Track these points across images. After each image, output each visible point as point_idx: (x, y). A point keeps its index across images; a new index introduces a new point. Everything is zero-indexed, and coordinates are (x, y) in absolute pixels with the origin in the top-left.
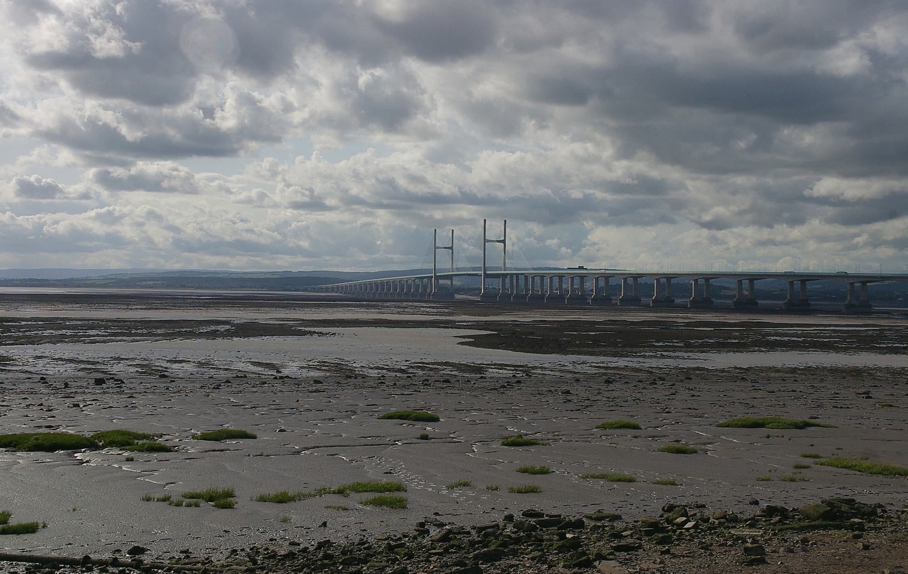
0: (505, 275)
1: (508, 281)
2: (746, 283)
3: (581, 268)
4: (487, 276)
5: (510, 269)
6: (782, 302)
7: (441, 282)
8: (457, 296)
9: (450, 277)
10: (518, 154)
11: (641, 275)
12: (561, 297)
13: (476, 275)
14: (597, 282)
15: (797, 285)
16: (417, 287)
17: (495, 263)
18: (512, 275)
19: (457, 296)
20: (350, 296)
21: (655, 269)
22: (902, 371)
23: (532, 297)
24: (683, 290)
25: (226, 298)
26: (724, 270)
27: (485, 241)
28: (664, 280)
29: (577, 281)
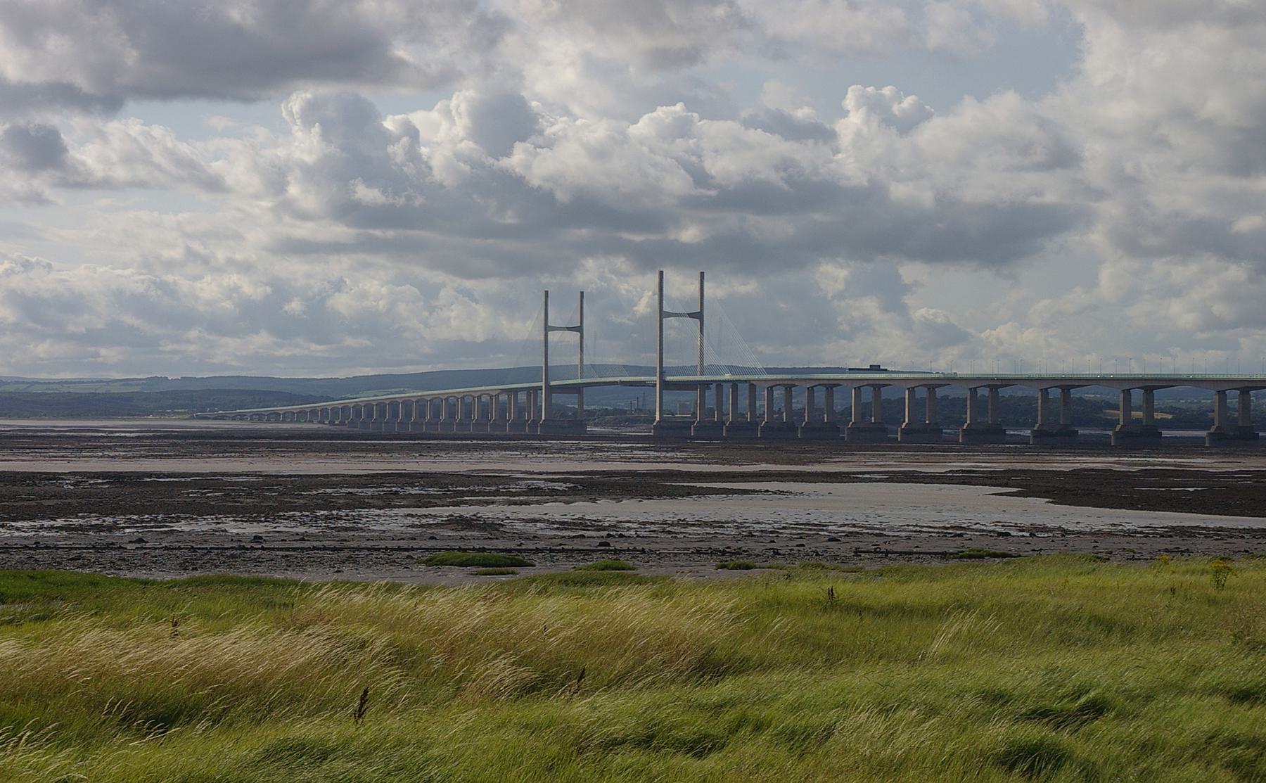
0: (705, 385)
1: (711, 395)
2: (1138, 396)
3: (875, 368)
4: (666, 385)
5: (716, 369)
6: (1203, 434)
7: (558, 398)
8: (1166, 433)
9: (577, 389)
10: (679, 107)
11: (1006, 382)
12: (833, 428)
13: (643, 384)
14: (858, 396)
15: (1233, 399)
16: (503, 411)
17: (681, 359)
18: (720, 384)
19: (1166, 433)
20: (345, 428)
21: (1111, 369)
22: (25, 589)
23: (734, 427)
24: (1094, 413)
25: (279, 435)
26: (1094, 372)
27: (662, 314)
28: (984, 392)
29: (820, 396)
